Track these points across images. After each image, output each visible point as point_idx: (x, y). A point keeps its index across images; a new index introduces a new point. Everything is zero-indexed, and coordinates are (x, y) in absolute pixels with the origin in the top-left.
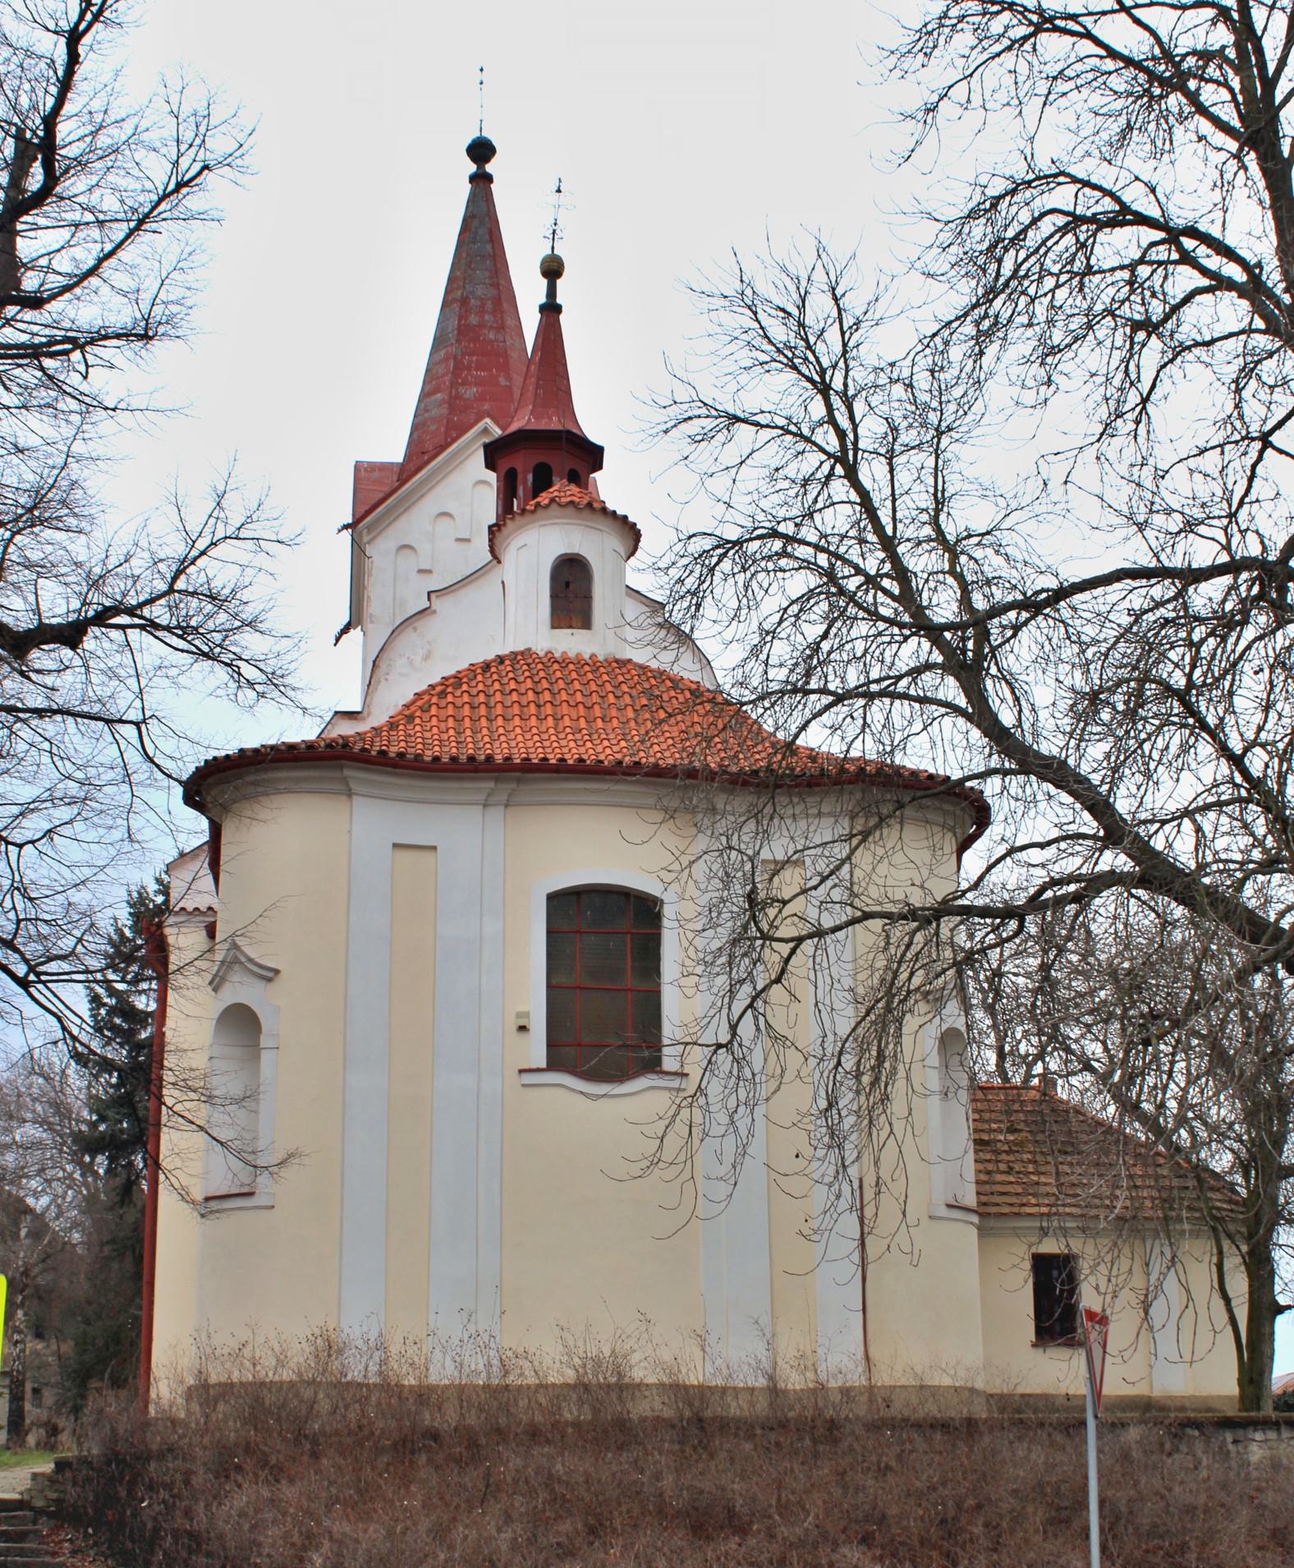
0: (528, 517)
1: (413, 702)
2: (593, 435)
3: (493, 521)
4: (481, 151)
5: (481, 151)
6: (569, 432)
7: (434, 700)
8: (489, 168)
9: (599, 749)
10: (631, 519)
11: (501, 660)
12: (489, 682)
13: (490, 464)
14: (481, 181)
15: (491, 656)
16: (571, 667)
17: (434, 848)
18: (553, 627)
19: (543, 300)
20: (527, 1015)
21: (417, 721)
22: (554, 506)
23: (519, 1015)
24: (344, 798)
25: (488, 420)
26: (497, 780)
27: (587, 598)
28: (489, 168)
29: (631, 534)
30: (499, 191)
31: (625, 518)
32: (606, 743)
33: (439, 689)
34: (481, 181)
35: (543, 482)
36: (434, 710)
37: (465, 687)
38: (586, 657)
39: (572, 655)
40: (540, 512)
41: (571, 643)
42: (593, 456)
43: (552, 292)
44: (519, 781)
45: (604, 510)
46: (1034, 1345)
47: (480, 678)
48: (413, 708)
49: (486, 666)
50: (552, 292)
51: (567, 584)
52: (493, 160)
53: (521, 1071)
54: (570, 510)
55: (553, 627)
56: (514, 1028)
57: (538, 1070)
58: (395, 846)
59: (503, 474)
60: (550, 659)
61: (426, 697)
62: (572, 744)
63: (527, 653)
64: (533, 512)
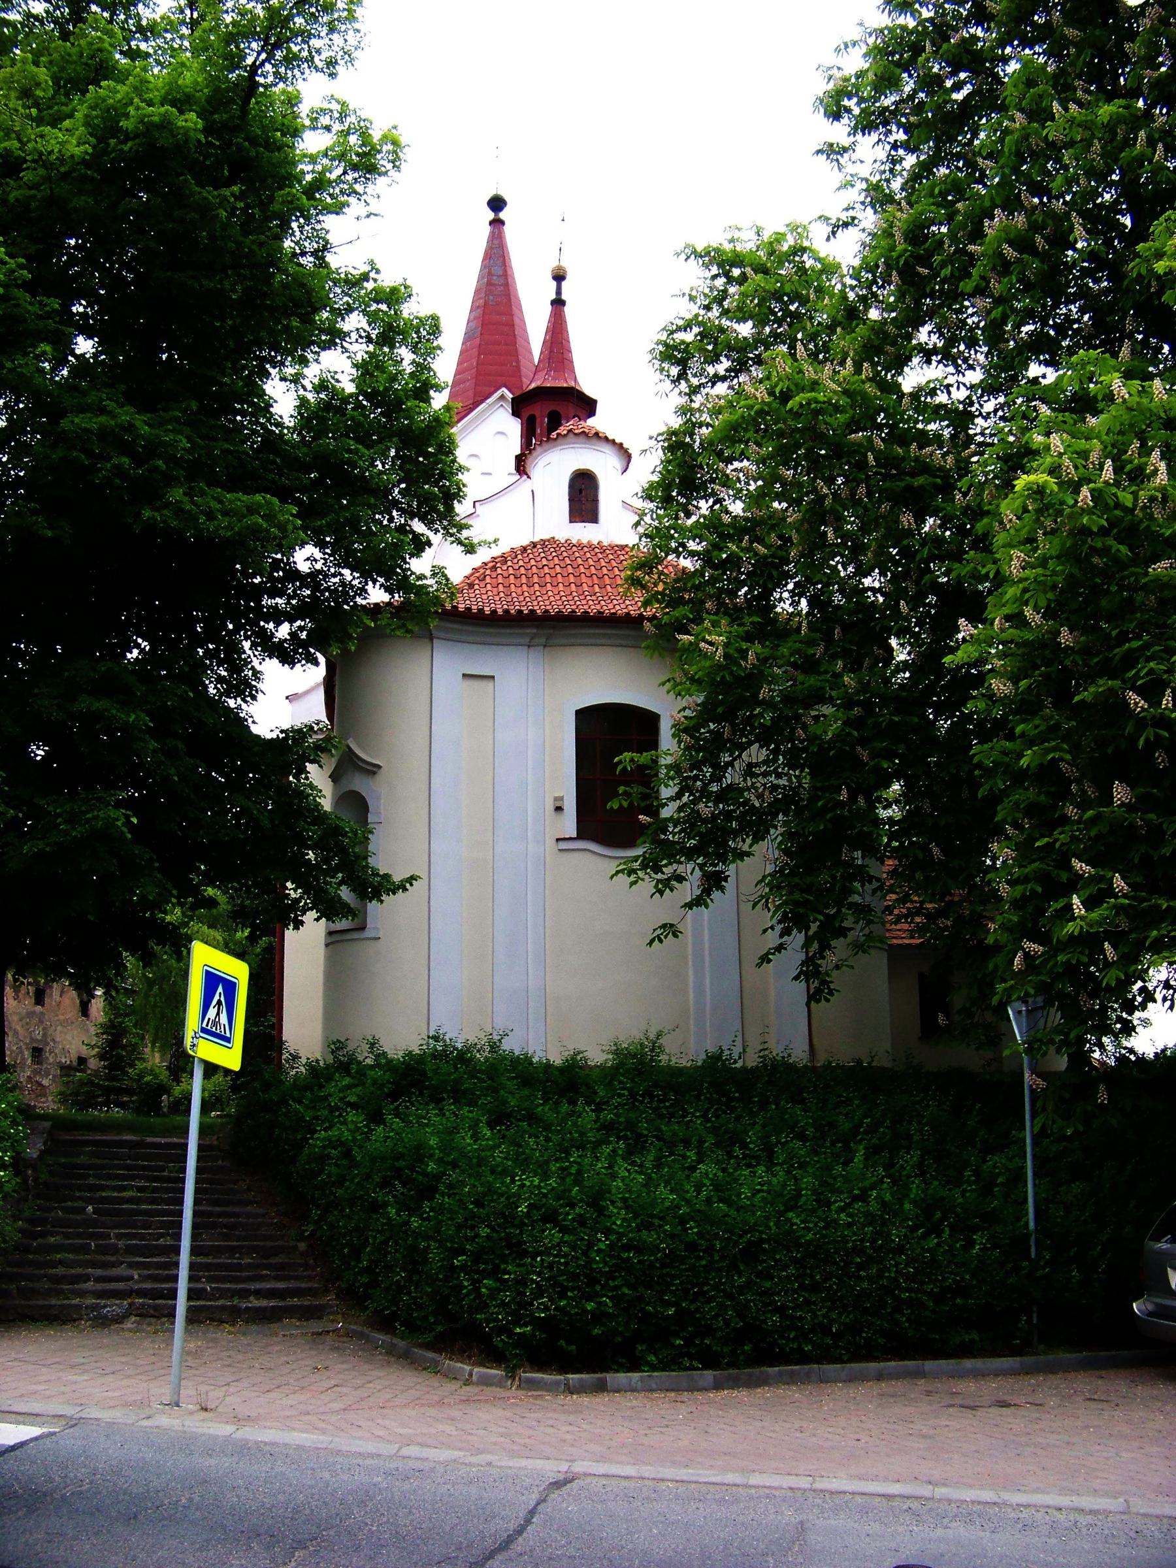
0: (550, 444)
1: (472, 574)
2: (588, 389)
3: (518, 452)
4: (497, 204)
5: (497, 204)
6: (573, 389)
7: (488, 572)
8: (502, 215)
9: (611, 606)
10: (625, 446)
11: (534, 545)
12: (527, 560)
13: (516, 413)
14: (497, 223)
15: (525, 543)
16: (586, 549)
17: (493, 677)
18: (571, 522)
19: (554, 296)
20: (561, 799)
21: (476, 587)
22: (571, 435)
23: (556, 799)
24: (427, 640)
25: (504, 389)
26: (537, 627)
27: (595, 501)
28: (502, 215)
29: (625, 455)
30: (510, 232)
31: (621, 445)
32: (615, 602)
33: (490, 565)
34: (497, 223)
35: (555, 422)
36: (488, 580)
37: (509, 563)
38: (595, 543)
39: (585, 541)
40: (560, 441)
41: (584, 533)
42: (588, 406)
43: (559, 291)
44: (554, 628)
45: (606, 439)
46: (920, 1038)
47: (520, 557)
48: (472, 578)
49: (524, 549)
50: (559, 291)
51: (581, 491)
52: (505, 210)
53: (558, 840)
54: (582, 439)
55: (571, 522)
56: (552, 809)
57: (570, 839)
58: (464, 675)
59: (525, 419)
60: (569, 544)
61: (482, 571)
62: (591, 603)
63: (553, 540)
64: (555, 439)
